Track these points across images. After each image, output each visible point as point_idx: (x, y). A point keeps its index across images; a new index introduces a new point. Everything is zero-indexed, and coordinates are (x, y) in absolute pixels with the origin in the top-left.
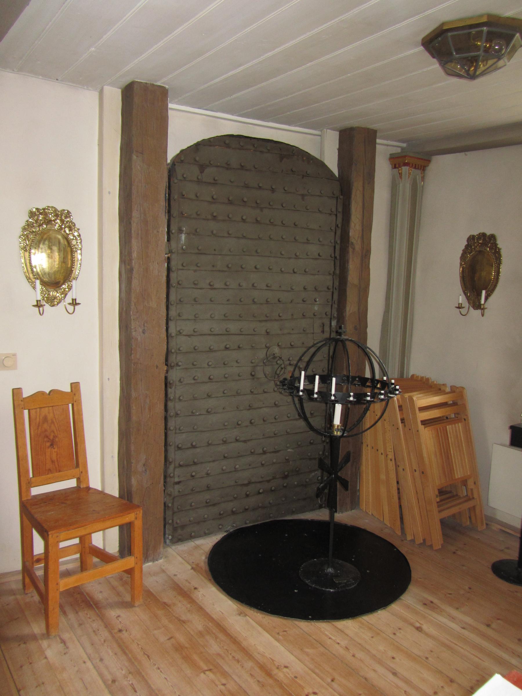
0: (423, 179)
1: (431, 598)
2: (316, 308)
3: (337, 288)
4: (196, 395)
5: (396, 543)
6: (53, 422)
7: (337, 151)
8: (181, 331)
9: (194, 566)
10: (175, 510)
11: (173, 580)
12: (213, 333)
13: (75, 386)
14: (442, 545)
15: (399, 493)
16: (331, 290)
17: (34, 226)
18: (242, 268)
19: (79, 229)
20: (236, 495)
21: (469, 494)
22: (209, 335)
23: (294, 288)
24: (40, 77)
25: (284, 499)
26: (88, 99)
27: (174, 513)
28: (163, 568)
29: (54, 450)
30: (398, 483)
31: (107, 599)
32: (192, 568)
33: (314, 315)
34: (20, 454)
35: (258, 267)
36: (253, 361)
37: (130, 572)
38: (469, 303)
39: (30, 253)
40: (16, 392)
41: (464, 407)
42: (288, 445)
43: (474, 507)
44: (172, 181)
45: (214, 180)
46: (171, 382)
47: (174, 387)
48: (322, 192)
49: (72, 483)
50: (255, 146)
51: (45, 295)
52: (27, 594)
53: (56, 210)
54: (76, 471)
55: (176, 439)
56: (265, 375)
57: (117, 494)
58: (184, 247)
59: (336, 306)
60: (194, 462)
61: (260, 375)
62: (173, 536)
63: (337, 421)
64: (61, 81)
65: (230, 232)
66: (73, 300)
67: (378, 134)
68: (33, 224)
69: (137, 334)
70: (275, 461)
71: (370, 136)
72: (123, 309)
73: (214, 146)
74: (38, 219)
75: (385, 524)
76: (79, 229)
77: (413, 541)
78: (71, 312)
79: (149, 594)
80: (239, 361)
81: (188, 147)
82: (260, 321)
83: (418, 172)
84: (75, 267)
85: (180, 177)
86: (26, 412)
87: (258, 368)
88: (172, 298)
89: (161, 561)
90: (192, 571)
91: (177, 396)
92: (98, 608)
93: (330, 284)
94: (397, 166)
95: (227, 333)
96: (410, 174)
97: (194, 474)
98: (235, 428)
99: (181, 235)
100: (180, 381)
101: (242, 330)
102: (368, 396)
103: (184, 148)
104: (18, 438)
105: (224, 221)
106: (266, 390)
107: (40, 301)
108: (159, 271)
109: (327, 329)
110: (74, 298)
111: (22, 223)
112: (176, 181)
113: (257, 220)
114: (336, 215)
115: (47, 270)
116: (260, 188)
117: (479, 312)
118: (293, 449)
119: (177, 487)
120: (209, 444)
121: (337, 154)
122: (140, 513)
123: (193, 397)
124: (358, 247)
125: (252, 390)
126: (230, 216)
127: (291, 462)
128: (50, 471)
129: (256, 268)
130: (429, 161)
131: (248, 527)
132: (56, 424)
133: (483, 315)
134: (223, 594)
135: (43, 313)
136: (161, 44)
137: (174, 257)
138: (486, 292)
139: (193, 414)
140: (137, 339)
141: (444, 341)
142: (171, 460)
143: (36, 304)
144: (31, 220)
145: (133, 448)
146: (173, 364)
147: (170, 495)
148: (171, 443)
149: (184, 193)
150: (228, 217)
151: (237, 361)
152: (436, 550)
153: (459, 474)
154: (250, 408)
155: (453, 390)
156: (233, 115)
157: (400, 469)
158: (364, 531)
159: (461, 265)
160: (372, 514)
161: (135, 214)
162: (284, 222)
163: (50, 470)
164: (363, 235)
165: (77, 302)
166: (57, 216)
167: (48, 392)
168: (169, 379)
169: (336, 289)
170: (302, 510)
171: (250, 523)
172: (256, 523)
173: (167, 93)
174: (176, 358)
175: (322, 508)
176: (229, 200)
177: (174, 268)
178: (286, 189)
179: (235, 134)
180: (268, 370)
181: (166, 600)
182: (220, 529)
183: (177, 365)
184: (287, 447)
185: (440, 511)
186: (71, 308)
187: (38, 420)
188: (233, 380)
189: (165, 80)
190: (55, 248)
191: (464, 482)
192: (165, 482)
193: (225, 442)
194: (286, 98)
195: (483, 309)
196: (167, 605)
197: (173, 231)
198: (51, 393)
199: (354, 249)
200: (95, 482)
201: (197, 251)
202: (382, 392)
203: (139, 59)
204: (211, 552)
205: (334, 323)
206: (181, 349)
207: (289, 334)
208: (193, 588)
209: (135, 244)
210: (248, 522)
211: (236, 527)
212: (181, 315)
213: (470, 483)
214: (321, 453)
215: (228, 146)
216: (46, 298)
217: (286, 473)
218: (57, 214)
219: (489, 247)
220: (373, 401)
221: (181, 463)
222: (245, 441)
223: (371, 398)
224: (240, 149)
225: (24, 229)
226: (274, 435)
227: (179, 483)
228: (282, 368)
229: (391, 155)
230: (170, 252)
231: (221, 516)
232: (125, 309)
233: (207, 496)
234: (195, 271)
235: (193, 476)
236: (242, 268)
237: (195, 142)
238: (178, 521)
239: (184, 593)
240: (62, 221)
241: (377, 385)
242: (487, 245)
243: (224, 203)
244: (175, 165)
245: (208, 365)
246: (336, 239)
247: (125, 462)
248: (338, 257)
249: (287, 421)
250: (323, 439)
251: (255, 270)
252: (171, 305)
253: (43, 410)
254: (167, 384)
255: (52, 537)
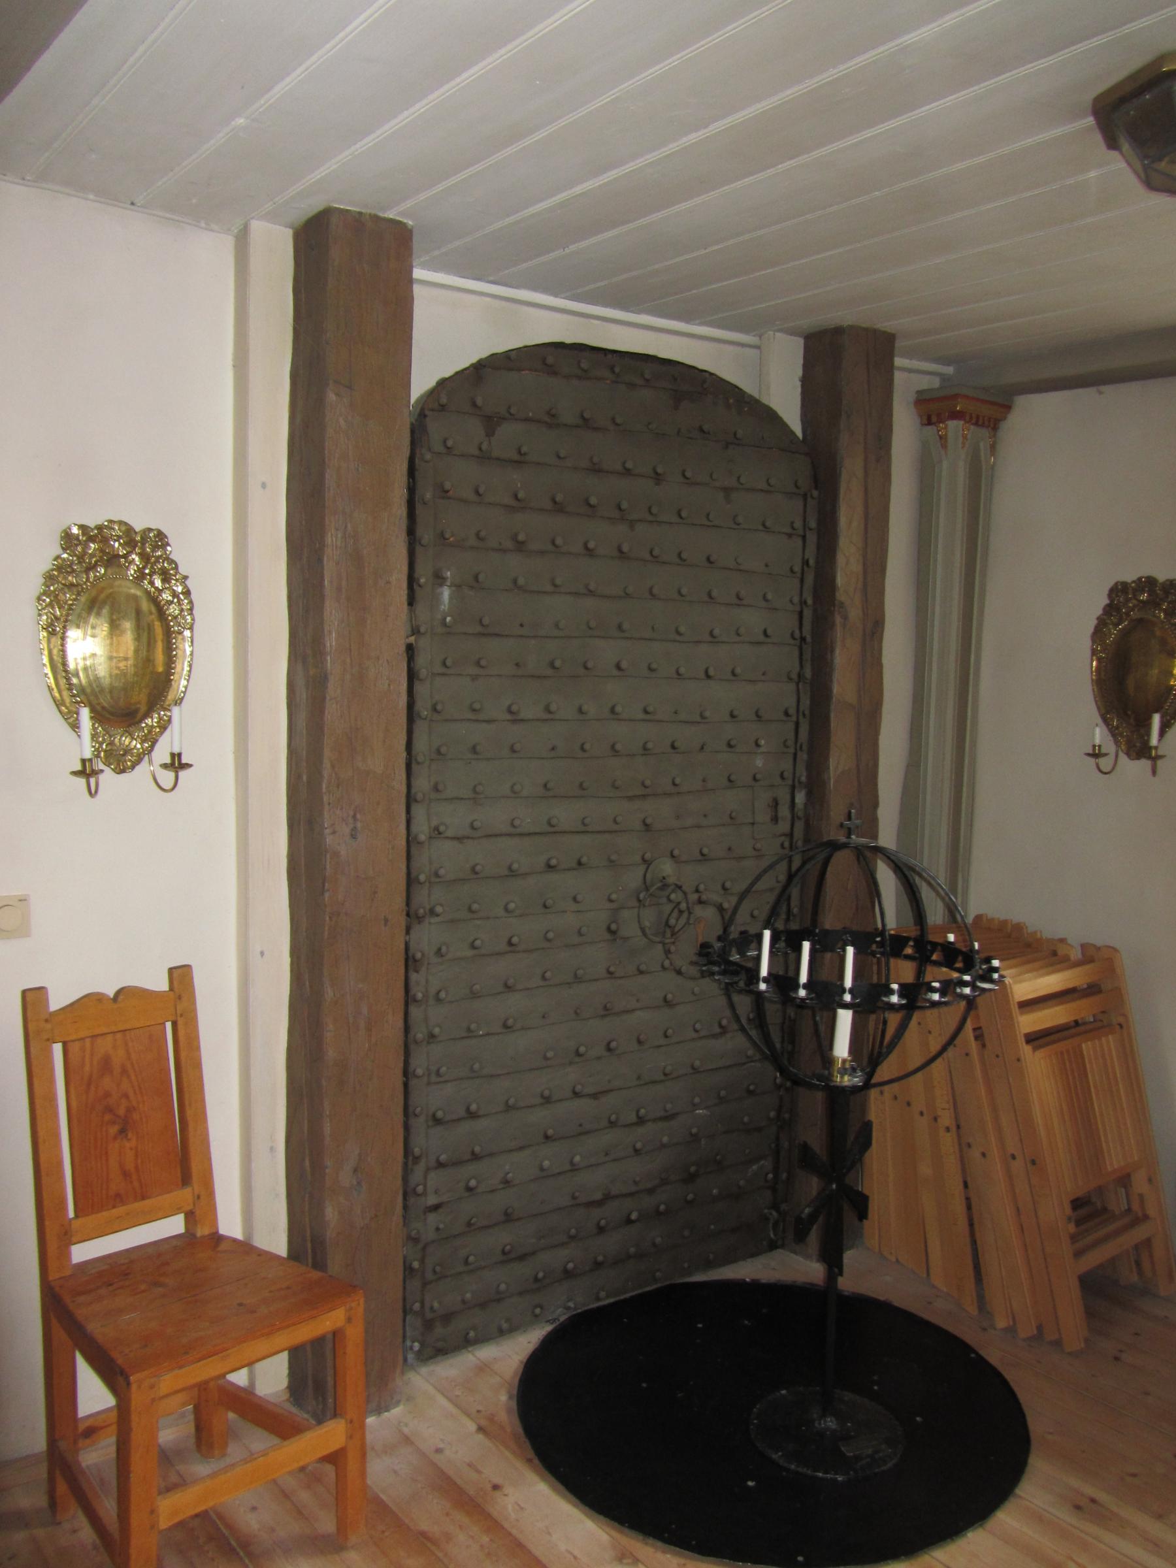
0: (993, 448)
1: (1090, 1490)
2: (759, 762)
3: (807, 713)
4: (477, 987)
5: (967, 1333)
6: (124, 1071)
7: (799, 384)
8: (442, 828)
9: (483, 1423)
10: (429, 1276)
11: (434, 1465)
12: (519, 830)
13: (181, 976)
14: (1086, 1340)
15: (969, 1207)
16: (794, 718)
17: (73, 571)
18: (586, 668)
19: (186, 578)
20: (573, 1231)
21: (1136, 1207)
22: (510, 835)
23: (707, 714)
24: (91, 197)
25: (686, 1233)
26: (211, 252)
27: (425, 1284)
28: (406, 1430)
29: (128, 1145)
30: (966, 1185)
31: (273, 1530)
32: (480, 1429)
33: (755, 779)
34: (43, 1158)
35: (624, 665)
36: (614, 896)
37: (334, 1458)
38: (1117, 743)
39: (63, 638)
40: (33, 999)
41: (1118, 994)
42: (697, 1100)
43: (1148, 1242)
44: (418, 455)
45: (520, 453)
46: (419, 955)
47: (424, 969)
48: (772, 482)
49: (174, 1225)
50: (617, 370)
51: (101, 744)
52: (60, 1523)
53: (129, 530)
54: (185, 1195)
55: (431, 1098)
56: (643, 930)
57: (282, 1250)
58: (448, 619)
59: (805, 756)
60: (473, 1153)
61: (630, 929)
62: (422, 1344)
63: (842, 1048)
64: (142, 206)
65: (558, 581)
66: (173, 755)
67: (898, 344)
68: (70, 566)
69: (336, 837)
70: (665, 1139)
71: (879, 347)
72: (299, 777)
73: (520, 370)
74: (84, 553)
75: (934, 1287)
76: (186, 578)
77: (1011, 1330)
78: (168, 786)
79: (381, 1509)
80: (579, 898)
81: (457, 373)
82: (630, 798)
83: (984, 433)
84: (178, 669)
85: (438, 447)
86: (58, 1049)
87: (625, 914)
88: (420, 745)
89: (397, 1412)
90: (481, 1436)
91: (432, 991)
92: (250, 1555)
93: (790, 702)
94: (934, 419)
95: (552, 830)
96: (965, 437)
97: (473, 1183)
98: (571, 1063)
99: (439, 590)
100: (438, 952)
101: (587, 821)
102: (934, 990)
103: (447, 375)
104: (38, 1117)
105: (542, 553)
106: (643, 967)
107: (90, 760)
108: (390, 679)
109: (784, 811)
110: (176, 751)
111: (45, 564)
112: (428, 456)
113: (620, 551)
114: (804, 537)
115: (106, 682)
116: (627, 472)
117: (1145, 764)
118: (706, 1108)
119: (432, 1218)
120: (508, 1108)
121: (799, 390)
122: (358, 1303)
123: (472, 992)
124: (855, 613)
125: (612, 969)
126: (559, 541)
127: (703, 1142)
128: (119, 1199)
129: (618, 667)
130: (1008, 408)
131: (604, 1306)
132: (133, 1078)
133: (1154, 772)
134: (569, 1502)
135: (96, 792)
136: (420, 107)
137: (423, 644)
138: (1162, 717)
139: (470, 1034)
140: (336, 854)
141: (1062, 839)
142: (417, 1151)
143: (79, 767)
144: (65, 556)
145: (327, 1129)
146: (421, 911)
147: (416, 1240)
148: (418, 1110)
149: (447, 485)
150: (553, 543)
151: (575, 899)
152: (1070, 1354)
153: (1114, 1161)
154: (607, 1011)
155: (1090, 955)
156: (556, 296)
157: (975, 1153)
158: (885, 1308)
159: (1094, 652)
160: (897, 1261)
161: (333, 539)
162: (684, 556)
163: (118, 1196)
164: (865, 585)
165: (184, 761)
166: (131, 544)
167: (111, 994)
168: (412, 945)
169: (804, 715)
170: (730, 1257)
171: (608, 1297)
172: (622, 1297)
173: (411, 239)
174: (429, 895)
175: (777, 1247)
176: (555, 502)
177: (423, 673)
178: (688, 474)
179: (569, 340)
180: (649, 917)
181: (424, 1525)
182: (536, 1316)
183: (432, 912)
184: (694, 1105)
185: (1078, 1254)
186: (167, 778)
187: (87, 1068)
188: (567, 946)
189: (403, 207)
190: (128, 625)
191: (1124, 1180)
192: (405, 1207)
193: (547, 1100)
194: (703, 252)
195: (1154, 759)
196: (429, 1539)
197: (422, 581)
198: (121, 997)
199: (845, 618)
200: (230, 1224)
201: (479, 629)
202: (967, 978)
203: (353, 148)
204: (520, 1381)
205: (800, 798)
206: (442, 872)
207: (699, 827)
208: (489, 1487)
209: (333, 615)
210: (602, 1294)
211: (575, 1309)
212: (440, 787)
213: (1140, 1183)
214: (772, 1114)
215: (552, 371)
216: (105, 751)
217: (693, 1169)
218: (131, 537)
219: (1165, 611)
220: (945, 1003)
221: (443, 1158)
222: (595, 1096)
223: (941, 996)
224: (579, 378)
225: (49, 578)
226: (662, 1078)
227: (436, 1208)
228: (681, 912)
229: (918, 392)
230: (415, 631)
231: (538, 1284)
232: (305, 778)
233: (503, 1237)
234: (474, 678)
235: (469, 1189)
236: (586, 668)
237: (474, 360)
238: (436, 1305)
239: (470, 1502)
240: (145, 557)
241: (932, 954)
242: (1157, 605)
243: (542, 510)
244: (425, 416)
245: (506, 909)
246: (805, 595)
247: (307, 1163)
248: (809, 639)
249: (693, 1040)
250: (778, 1081)
251: (615, 672)
252: (418, 763)
253: (99, 1040)
254: (411, 962)
255: (139, 1387)
